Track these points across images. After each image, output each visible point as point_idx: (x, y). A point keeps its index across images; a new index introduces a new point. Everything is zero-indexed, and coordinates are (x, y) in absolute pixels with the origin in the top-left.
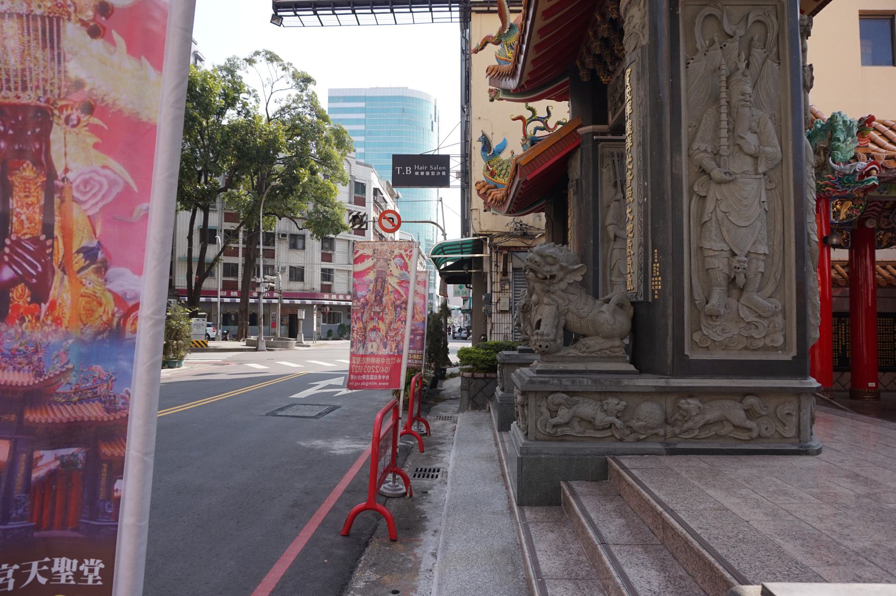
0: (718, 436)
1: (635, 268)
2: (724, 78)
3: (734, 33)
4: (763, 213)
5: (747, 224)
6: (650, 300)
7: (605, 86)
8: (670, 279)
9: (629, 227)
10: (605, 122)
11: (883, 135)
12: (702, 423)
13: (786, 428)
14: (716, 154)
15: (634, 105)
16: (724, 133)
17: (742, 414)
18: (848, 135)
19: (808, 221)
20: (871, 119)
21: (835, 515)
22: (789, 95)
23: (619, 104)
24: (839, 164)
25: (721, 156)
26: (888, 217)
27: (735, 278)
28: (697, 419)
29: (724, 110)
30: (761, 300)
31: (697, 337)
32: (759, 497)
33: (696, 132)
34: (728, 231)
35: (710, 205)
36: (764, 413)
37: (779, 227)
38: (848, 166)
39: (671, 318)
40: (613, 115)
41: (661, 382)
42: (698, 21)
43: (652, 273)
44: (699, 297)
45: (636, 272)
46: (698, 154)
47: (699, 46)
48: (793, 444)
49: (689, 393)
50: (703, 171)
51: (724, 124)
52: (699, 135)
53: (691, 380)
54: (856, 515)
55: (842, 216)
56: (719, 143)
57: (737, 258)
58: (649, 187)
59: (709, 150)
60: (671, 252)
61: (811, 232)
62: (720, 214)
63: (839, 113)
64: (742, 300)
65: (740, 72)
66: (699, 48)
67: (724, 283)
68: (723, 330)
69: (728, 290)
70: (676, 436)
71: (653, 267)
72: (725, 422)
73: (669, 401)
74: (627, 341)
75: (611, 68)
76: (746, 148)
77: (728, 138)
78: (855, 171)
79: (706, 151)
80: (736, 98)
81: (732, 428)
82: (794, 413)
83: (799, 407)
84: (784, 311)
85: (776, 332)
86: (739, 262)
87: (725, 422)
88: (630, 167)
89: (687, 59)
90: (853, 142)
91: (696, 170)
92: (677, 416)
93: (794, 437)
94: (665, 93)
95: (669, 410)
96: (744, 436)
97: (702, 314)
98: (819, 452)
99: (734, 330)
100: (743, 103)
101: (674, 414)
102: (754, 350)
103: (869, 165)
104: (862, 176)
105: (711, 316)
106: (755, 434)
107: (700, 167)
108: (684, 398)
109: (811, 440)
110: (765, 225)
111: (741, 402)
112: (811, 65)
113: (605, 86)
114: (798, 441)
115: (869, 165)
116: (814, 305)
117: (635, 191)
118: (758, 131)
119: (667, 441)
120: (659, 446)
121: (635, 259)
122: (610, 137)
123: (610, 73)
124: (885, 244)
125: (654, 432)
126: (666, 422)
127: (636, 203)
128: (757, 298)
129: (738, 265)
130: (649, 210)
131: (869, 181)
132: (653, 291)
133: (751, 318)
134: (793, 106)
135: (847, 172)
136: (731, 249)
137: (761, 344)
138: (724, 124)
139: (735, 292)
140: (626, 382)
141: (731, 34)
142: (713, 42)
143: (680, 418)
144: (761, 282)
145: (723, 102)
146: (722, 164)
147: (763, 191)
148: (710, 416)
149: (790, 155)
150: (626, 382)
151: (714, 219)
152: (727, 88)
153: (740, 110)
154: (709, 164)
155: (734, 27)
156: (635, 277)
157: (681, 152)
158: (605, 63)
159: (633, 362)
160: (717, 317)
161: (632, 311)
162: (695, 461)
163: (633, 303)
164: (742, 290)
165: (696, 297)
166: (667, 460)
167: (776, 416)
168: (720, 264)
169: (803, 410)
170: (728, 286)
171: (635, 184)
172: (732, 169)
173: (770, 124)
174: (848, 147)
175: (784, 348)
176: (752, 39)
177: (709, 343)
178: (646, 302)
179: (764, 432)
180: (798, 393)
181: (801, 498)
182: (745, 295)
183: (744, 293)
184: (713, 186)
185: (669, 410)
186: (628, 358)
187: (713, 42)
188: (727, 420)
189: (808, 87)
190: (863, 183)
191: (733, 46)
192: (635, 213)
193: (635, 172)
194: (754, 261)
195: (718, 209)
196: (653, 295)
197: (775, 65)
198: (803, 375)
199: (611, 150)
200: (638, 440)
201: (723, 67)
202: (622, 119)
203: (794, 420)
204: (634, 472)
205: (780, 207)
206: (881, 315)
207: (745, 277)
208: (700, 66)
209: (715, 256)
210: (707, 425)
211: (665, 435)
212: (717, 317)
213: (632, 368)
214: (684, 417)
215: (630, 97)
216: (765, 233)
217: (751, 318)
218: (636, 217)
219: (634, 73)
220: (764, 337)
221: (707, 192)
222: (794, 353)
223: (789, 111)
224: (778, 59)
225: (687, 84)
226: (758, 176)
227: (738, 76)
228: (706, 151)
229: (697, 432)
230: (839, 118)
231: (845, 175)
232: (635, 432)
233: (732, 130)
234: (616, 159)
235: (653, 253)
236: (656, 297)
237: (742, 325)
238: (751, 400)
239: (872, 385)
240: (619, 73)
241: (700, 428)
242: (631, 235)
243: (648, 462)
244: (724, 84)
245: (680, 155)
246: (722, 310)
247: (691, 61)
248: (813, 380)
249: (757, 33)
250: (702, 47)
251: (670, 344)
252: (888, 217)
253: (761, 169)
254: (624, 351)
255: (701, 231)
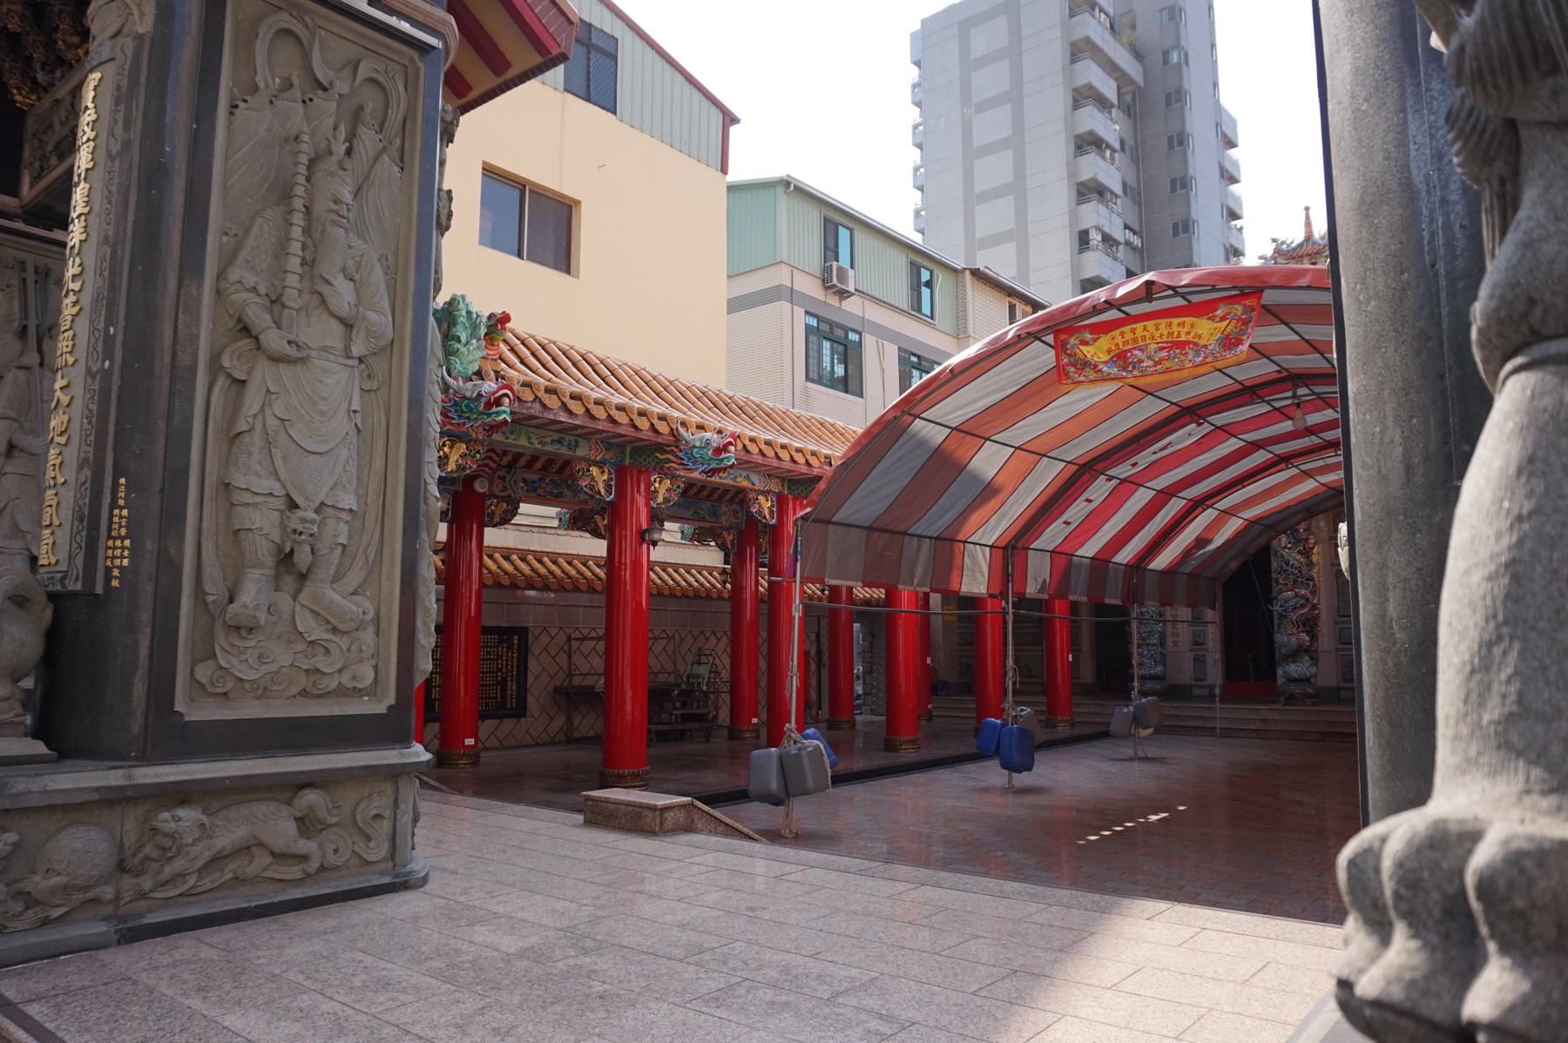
0: (238, 881)
1: (67, 514)
2: (304, 159)
3: (331, 83)
4: (353, 432)
5: (322, 448)
6: (99, 590)
7: (21, 114)
8: (150, 545)
9: (57, 422)
10: (14, 191)
11: (512, 350)
12: (206, 856)
13: (371, 844)
14: (275, 302)
15: (101, 153)
16: (294, 263)
17: (291, 827)
18: (472, 335)
19: (427, 459)
20: (505, 318)
21: (481, 1011)
22: (414, 229)
23: (53, 161)
24: (456, 379)
25: (284, 306)
26: (504, 479)
27: (292, 552)
28: (195, 850)
29: (298, 219)
30: (337, 598)
31: (203, 672)
32: (338, 1007)
33: (237, 248)
34: (285, 458)
35: (252, 400)
36: (335, 820)
37: (378, 463)
38: (470, 385)
39: (148, 631)
40: (36, 179)
41: (113, 777)
42: (265, 32)
43: (110, 529)
44: (214, 589)
45: (67, 526)
46: (237, 291)
47: (259, 79)
48: (383, 873)
49: (181, 795)
50: (245, 330)
51: (296, 247)
52: (244, 254)
53: (184, 767)
54: (516, 1000)
55: (451, 466)
56: (283, 280)
57: (300, 513)
58: (120, 338)
59: (262, 291)
60: (157, 485)
61: (429, 480)
62: (271, 422)
63: (463, 297)
64: (304, 598)
65: (334, 159)
66: (262, 86)
67: (270, 562)
68: (261, 657)
69: (277, 577)
70: (144, 896)
71: (111, 516)
72: (254, 849)
73: (130, 822)
74: (28, 683)
75: (41, 77)
76: (333, 302)
77: (302, 277)
78: (480, 395)
79: (254, 290)
80: (322, 205)
81: (269, 860)
82: (387, 814)
83: (396, 800)
84: (377, 620)
85: (361, 661)
86: (303, 520)
87: (254, 849)
88: (72, 286)
89: (232, 98)
90: (478, 348)
91: (231, 324)
92: (149, 850)
93: (386, 859)
94: (177, 149)
95: (130, 838)
96: (294, 872)
97: (219, 624)
98: (424, 881)
99: (282, 657)
100: (337, 218)
101: (143, 846)
102: (319, 696)
103: (500, 389)
104: (489, 405)
105: (238, 628)
106: (313, 866)
107: (240, 320)
108: (168, 808)
109: (411, 860)
110: (354, 456)
111: (289, 803)
112: (449, 192)
113: (21, 114)
114: (390, 864)
115: (500, 389)
116: (427, 610)
117: (83, 340)
118: (357, 277)
119: (122, 911)
120: (101, 928)
121: (68, 495)
122: (19, 225)
123: (39, 89)
124: (497, 519)
125: (90, 895)
126: (121, 867)
127: (81, 367)
128: (332, 595)
129: (300, 528)
130: (115, 389)
131: (498, 413)
132: (108, 570)
133: (318, 633)
134: (419, 251)
135: (468, 394)
136: (288, 495)
137: (333, 684)
138: (296, 247)
139: (289, 582)
140: (20, 785)
141: (326, 84)
142: (288, 85)
143: (154, 854)
144: (339, 564)
145: (298, 204)
146: (284, 323)
147: (357, 393)
148: (226, 839)
149: (408, 336)
150: (20, 785)
151: (259, 429)
152: (308, 180)
153: (329, 229)
154: (259, 317)
155: (331, 74)
156: (63, 536)
157: (201, 278)
158: (29, 60)
159: (40, 731)
160: (251, 630)
161: (47, 614)
162: (187, 946)
163: (52, 597)
164: (303, 577)
165: (208, 587)
166: (121, 959)
167: (355, 822)
168: (264, 523)
169: (402, 807)
170: (277, 569)
171: (83, 327)
172: (302, 338)
173: (378, 271)
174: (471, 355)
175: (373, 691)
176: (361, 108)
177: (229, 686)
178: (88, 595)
179: (332, 859)
180: (394, 774)
181: (417, 989)
182: (309, 588)
183: (308, 583)
184: (263, 364)
185: (130, 838)
186: (28, 720)
187: (288, 85)
188: (261, 844)
189: (443, 228)
190: (489, 415)
191: (327, 106)
192: (78, 390)
193: (86, 299)
194: (331, 522)
195: (268, 412)
196: (108, 576)
197: (396, 169)
198: (402, 740)
199: (22, 255)
200: (46, 922)
201: (305, 138)
202: (66, 186)
203: (386, 825)
204: (34, 1010)
205: (384, 426)
206: (486, 630)
207: (313, 552)
208: (258, 121)
209: (255, 504)
210: (218, 860)
211: (117, 898)
212: (251, 630)
213: (40, 748)
214: (165, 849)
215: (90, 134)
216: (354, 470)
217: (318, 633)
218: (79, 401)
219: (109, 85)
220: (340, 671)
221: (249, 373)
222: (391, 699)
223: (412, 256)
224: (402, 160)
225: (228, 147)
226: (350, 362)
227: (330, 164)
228: (254, 290)
229: (192, 880)
230: (462, 306)
231: (464, 398)
232: (38, 903)
233: (309, 263)
234: (31, 277)
235: (115, 485)
236: (115, 583)
237: (300, 647)
238: (311, 797)
239: (470, 742)
240: (62, 92)
241: (199, 870)
242: (62, 440)
243: (72, 972)
244: (302, 169)
245: (200, 287)
246: (262, 617)
247: (242, 105)
248: (418, 747)
249: (371, 102)
250: (267, 86)
251: (139, 689)
252: (504, 479)
253: (357, 350)
254: (19, 710)
255: (230, 449)
